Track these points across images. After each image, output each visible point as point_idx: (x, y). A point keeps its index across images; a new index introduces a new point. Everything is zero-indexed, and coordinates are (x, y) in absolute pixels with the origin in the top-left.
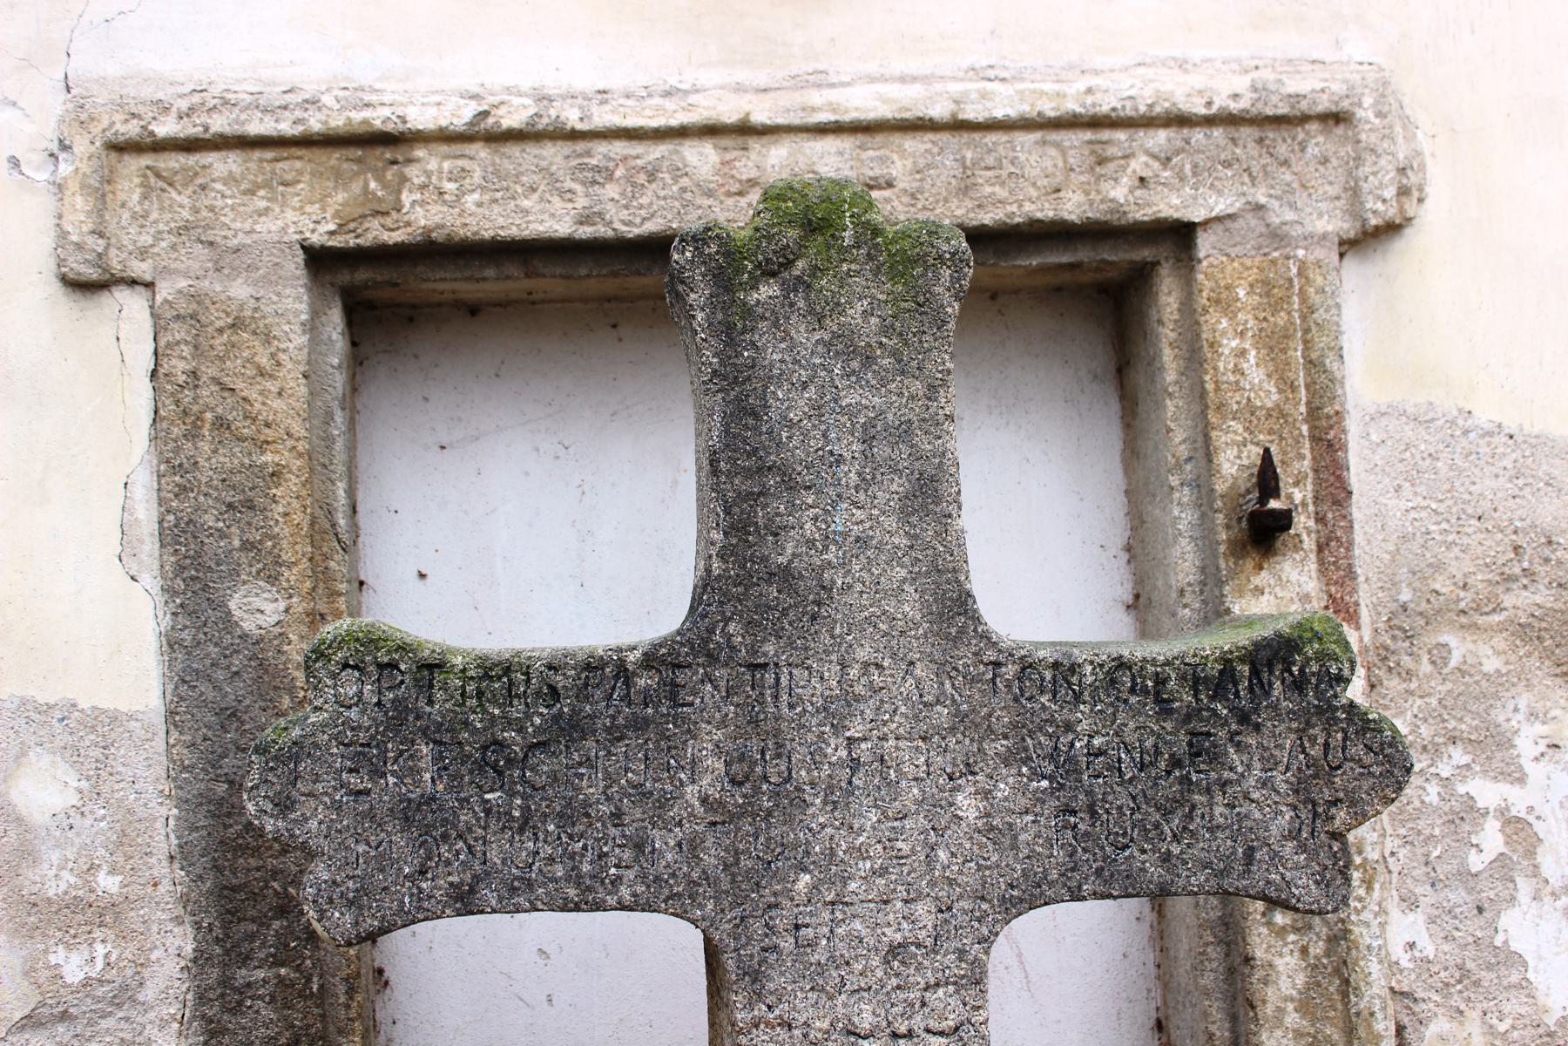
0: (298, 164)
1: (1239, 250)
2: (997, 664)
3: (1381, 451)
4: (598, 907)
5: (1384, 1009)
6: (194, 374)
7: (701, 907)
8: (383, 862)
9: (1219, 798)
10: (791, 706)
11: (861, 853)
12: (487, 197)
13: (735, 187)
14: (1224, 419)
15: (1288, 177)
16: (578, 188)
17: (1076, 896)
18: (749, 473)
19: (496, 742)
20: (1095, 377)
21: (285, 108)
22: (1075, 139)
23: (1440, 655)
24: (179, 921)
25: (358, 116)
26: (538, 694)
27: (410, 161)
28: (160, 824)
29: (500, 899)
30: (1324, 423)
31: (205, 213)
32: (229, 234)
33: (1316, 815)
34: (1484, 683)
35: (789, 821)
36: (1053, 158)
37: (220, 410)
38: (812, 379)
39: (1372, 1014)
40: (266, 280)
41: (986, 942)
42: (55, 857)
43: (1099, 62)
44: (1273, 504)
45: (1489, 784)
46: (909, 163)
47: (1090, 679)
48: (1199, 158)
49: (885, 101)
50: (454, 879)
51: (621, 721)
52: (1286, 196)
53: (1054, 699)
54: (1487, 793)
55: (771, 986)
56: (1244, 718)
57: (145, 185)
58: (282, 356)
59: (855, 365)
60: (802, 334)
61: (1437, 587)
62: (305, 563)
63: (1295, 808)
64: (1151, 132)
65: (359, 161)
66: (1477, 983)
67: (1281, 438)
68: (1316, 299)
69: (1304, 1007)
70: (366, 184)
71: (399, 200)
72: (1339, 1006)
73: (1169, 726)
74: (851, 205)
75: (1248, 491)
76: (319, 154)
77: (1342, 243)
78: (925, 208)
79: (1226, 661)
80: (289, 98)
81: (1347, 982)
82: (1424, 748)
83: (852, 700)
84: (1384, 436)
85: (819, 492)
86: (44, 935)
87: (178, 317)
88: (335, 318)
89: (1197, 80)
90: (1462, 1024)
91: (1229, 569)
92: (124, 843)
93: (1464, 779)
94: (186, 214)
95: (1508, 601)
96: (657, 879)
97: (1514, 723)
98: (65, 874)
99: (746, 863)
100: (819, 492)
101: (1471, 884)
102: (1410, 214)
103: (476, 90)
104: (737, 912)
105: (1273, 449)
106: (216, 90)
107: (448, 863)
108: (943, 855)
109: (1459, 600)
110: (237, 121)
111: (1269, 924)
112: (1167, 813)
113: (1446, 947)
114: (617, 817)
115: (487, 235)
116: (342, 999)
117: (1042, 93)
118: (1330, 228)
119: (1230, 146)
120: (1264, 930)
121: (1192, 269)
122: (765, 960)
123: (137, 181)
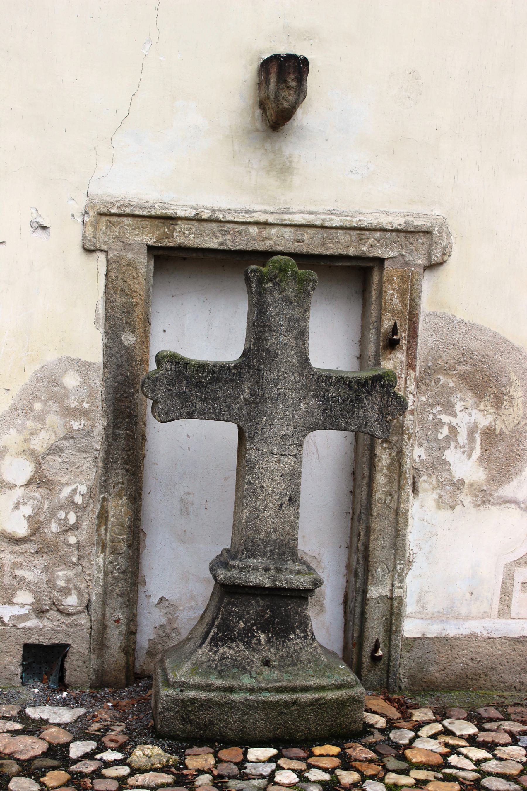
0: (147, 223)
1: (396, 267)
2: (313, 375)
3: (428, 325)
4: (219, 420)
5: (409, 471)
6: (117, 277)
7: (242, 422)
8: (173, 405)
9: (361, 410)
10: (266, 380)
11: (278, 414)
12: (196, 236)
13: (262, 239)
14: (386, 312)
15: (412, 248)
16: (220, 235)
17: (325, 429)
18: (261, 326)
19: (200, 382)
20: (356, 292)
21: (145, 208)
22: (354, 233)
23: (437, 381)
24: (103, 417)
25: (164, 212)
26: (210, 372)
27: (176, 224)
28: (100, 392)
29: (198, 416)
30: (413, 316)
31: (122, 234)
32: (128, 240)
33: (383, 416)
34: (449, 390)
35: (263, 405)
36: (348, 238)
37: (122, 287)
38: (278, 306)
39: (406, 472)
40: (137, 253)
41: (304, 437)
42: (73, 398)
43: (364, 211)
44: (395, 337)
45: (446, 416)
46: (309, 236)
47: (334, 380)
48: (388, 241)
49: (304, 219)
50: (188, 410)
51: (228, 379)
52: (411, 253)
53: (325, 384)
54: (445, 418)
55: (255, 441)
56: (369, 393)
57: (107, 225)
58: (140, 274)
59: (288, 304)
60: (277, 296)
61: (439, 362)
62: (141, 329)
63: (378, 414)
64: (376, 232)
65: (163, 223)
66: (436, 468)
67: (401, 319)
68: (415, 282)
69: (388, 468)
70: (165, 230)
71: (173, 235)
72: (398, 469)
73: (351, 393)
74: (291, 266)
75: (390, 332)
76: (153, 221)
77: (425, 267)
78: (312, 249)
79: (366, 380)
80: (146, 204)
81: (400, 463)
82: (430, 405)
83: (279, 380)
84: (430, 320)
85: (277, 332)
86: (69, 417)
87: (114, 262)
88: (152, 262)
89: (390, 219)
90: (431, 478)
91: (382, 353)
92: (91, 396)
93: (440, 415)
94: (117, 234)
95: (459, 368)
96: (233, 415)
97: (455, 401)
98: (75, 402)
99: (252, 413)
100: (277, 332)
101: (438, 442)
102: (445, 259)
103: (195, 206)
104: (249, 424)
105: (398, 322)
106: (126, 201)
107: (187, 407)
108: (296, 416)
109: (445, 367)
110: (132, 210)
111: (382, 446)
112: (348, 412)
113: (429, 458)
114: (225, 400)
115: (195, 246)
116: (141, 441)
117: (347, 220)
118: (422, 263)
119: (397, 238)
120: (380, 448)
121: (383, 270)
122: (254, 435)
123: (105, 223)
